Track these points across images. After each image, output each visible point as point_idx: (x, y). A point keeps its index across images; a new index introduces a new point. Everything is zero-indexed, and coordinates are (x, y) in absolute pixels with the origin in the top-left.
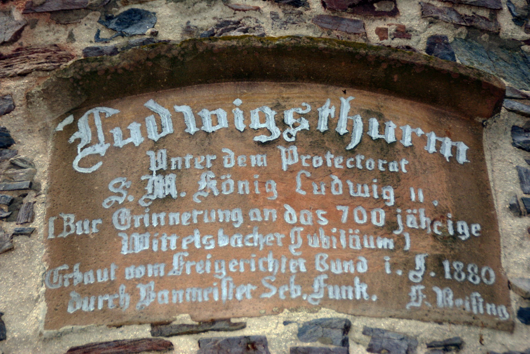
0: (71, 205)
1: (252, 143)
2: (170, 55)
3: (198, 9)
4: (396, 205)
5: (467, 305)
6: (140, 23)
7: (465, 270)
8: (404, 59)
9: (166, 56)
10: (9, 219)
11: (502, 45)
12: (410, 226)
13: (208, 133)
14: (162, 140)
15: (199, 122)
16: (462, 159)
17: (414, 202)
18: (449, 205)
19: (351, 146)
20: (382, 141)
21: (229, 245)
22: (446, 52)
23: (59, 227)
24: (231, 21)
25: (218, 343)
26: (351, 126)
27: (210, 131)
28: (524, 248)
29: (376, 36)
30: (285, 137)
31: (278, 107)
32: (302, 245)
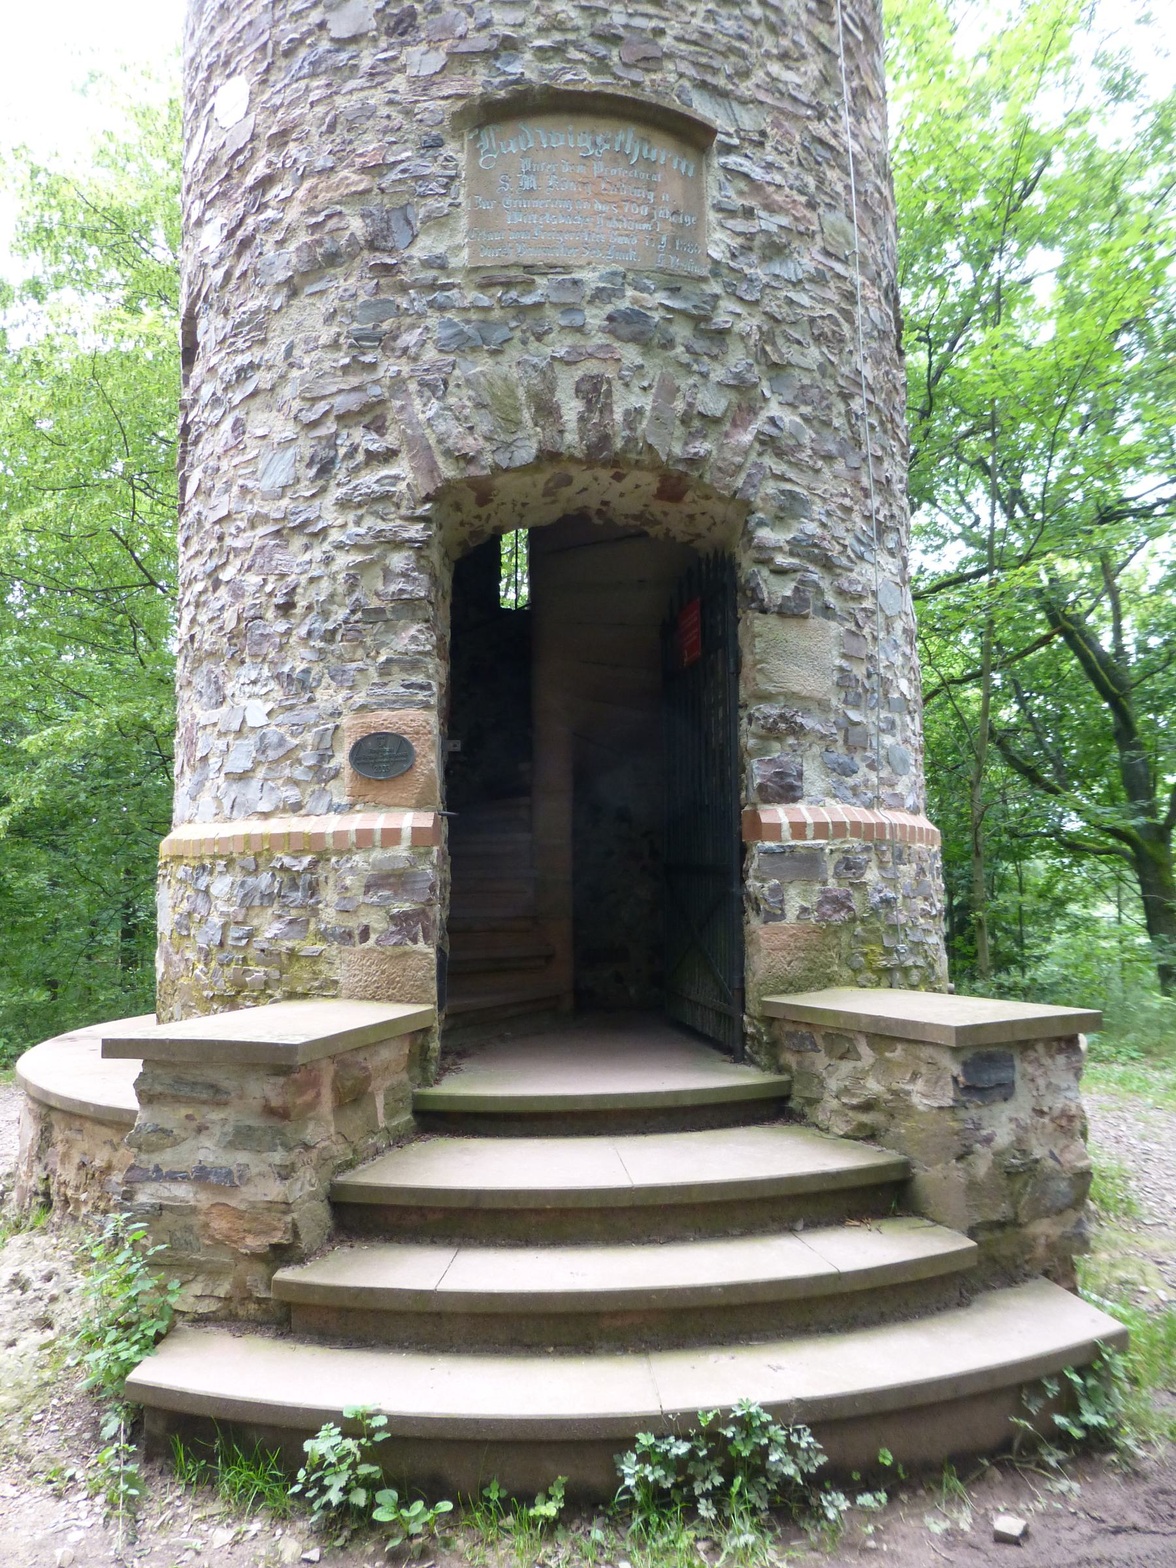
16: (690, 174)
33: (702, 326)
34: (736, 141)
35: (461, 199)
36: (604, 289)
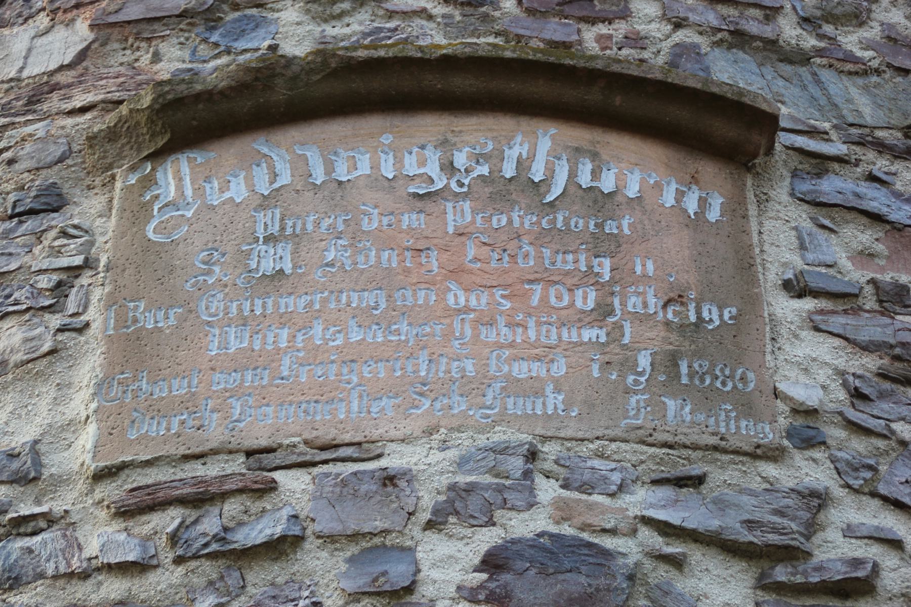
0: (141, 287)
1: (404, 194)
2: (289, 73)
3: (338, 11)
4: (613, 281)
5: (712, 421)
6: (254, 34)
7: (711, 372)
8: (630, 72)
9: (283, 75)
10: (52, 309)
11: (782, 57)
12: (630, 309)
13: (340, 183)
14: (273, 193)
15: (330, 168)
16: (714, 215)
17: (639, 276)
18: (692, 280)
19: (549, 198)
20: (596, 191)
21: (364, 339)
22: (697, 66)
23: (122, 322)
24: (384, 28)
25: (341, 477)
26: (551, 172)
27: (344, 179)
28: (802, 340)
29: (595, 45)
30: (454, 186)
31: (444, 144)
32: (472, 337)
33: (781, 574)
34: (837, 148)
35: (92, 314)
36: (470, 489)
